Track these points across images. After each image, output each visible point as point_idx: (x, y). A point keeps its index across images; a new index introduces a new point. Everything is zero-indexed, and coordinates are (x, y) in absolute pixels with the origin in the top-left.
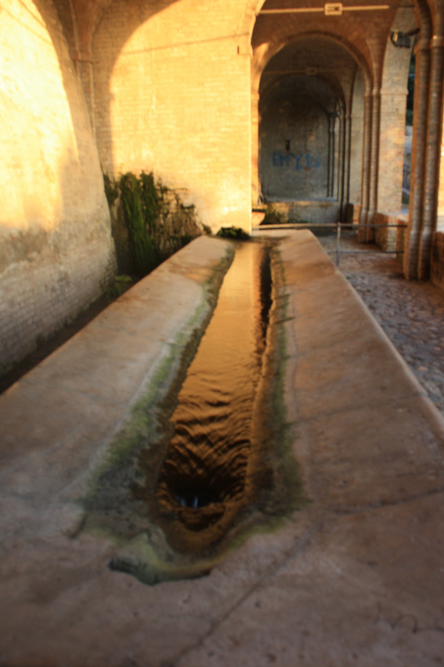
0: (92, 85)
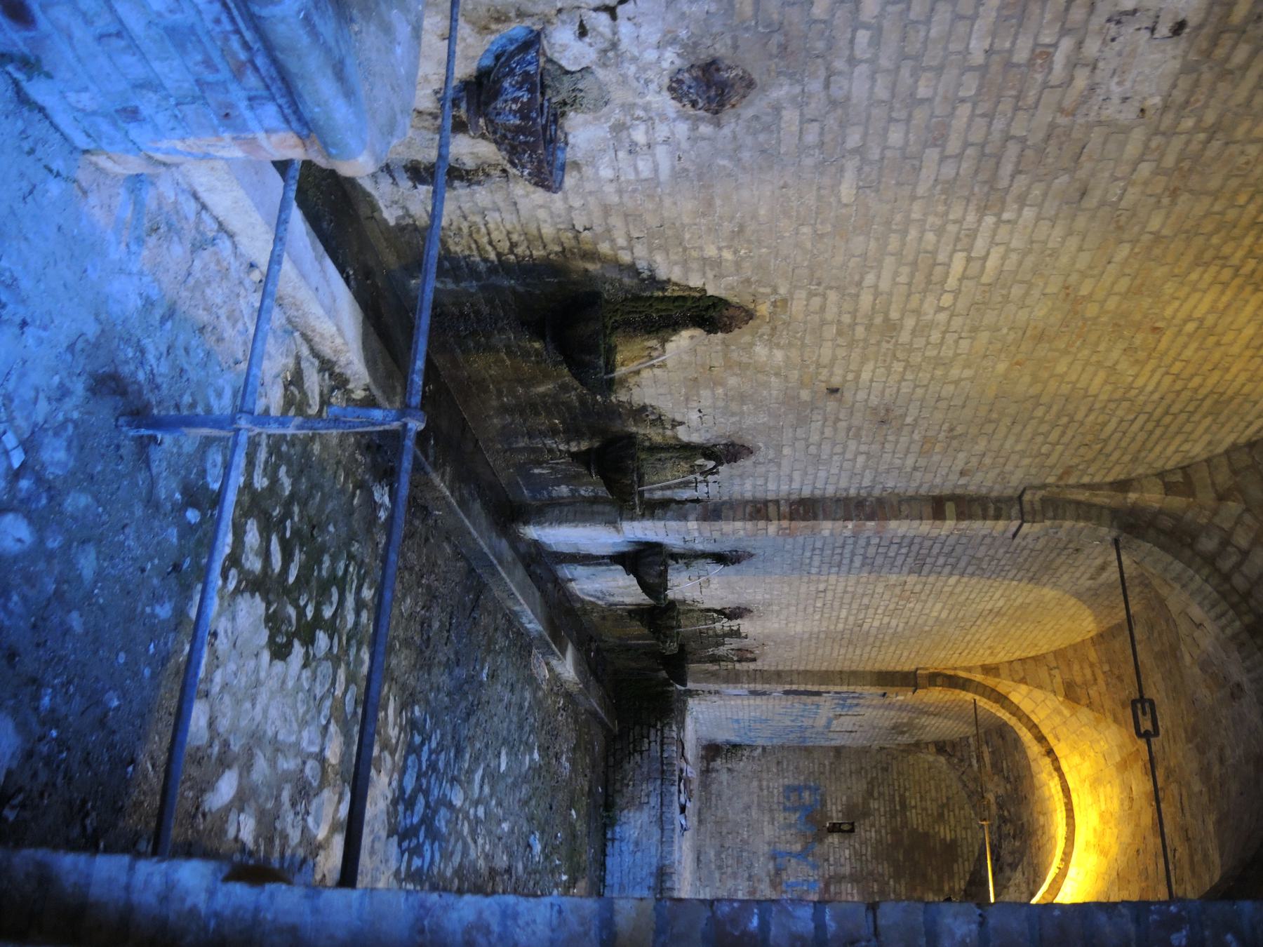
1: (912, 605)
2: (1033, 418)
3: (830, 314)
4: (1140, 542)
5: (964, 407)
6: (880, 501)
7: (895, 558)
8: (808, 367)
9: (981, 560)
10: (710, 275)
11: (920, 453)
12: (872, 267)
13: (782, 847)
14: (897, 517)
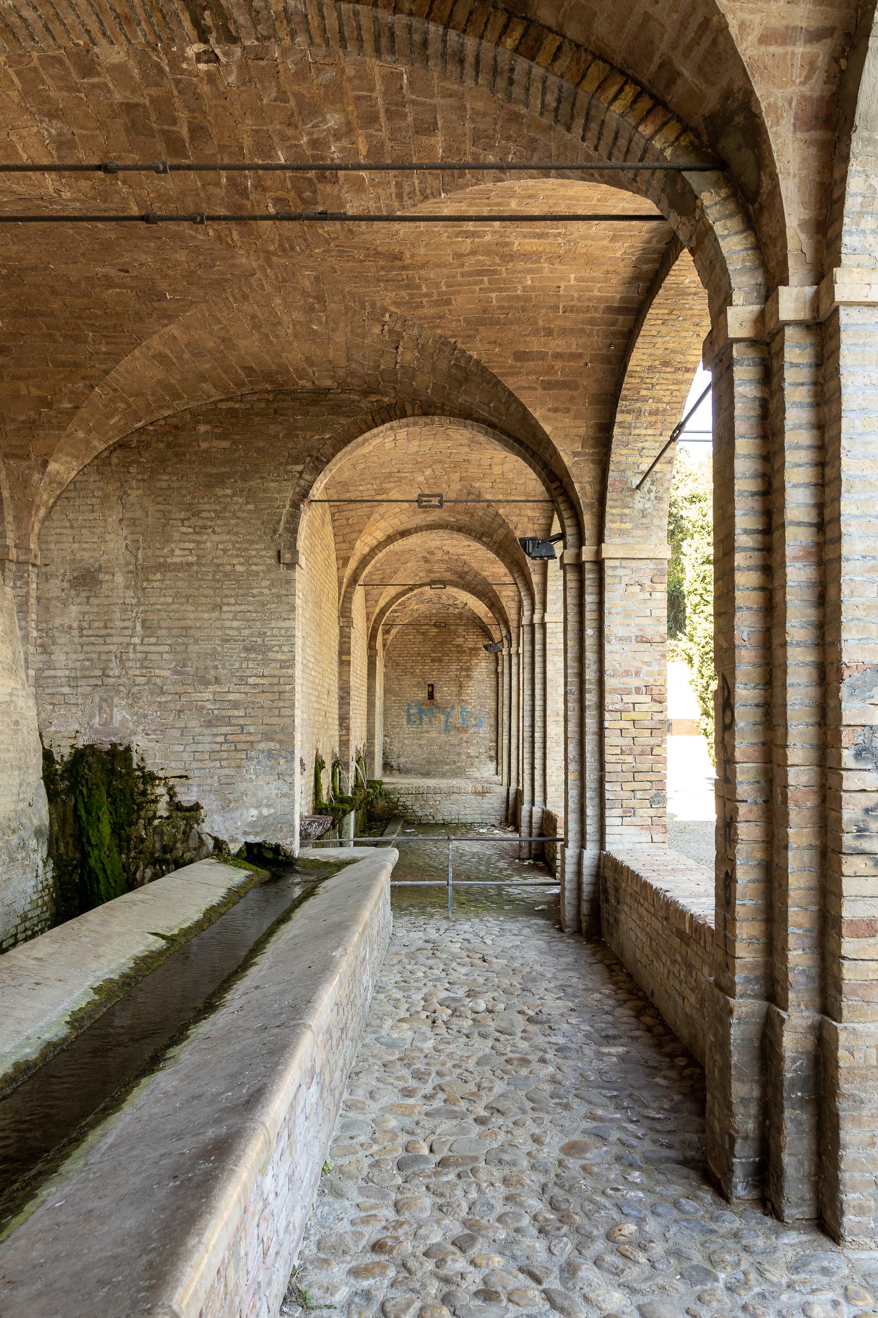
0: (33, 601)
13: (443, 727)
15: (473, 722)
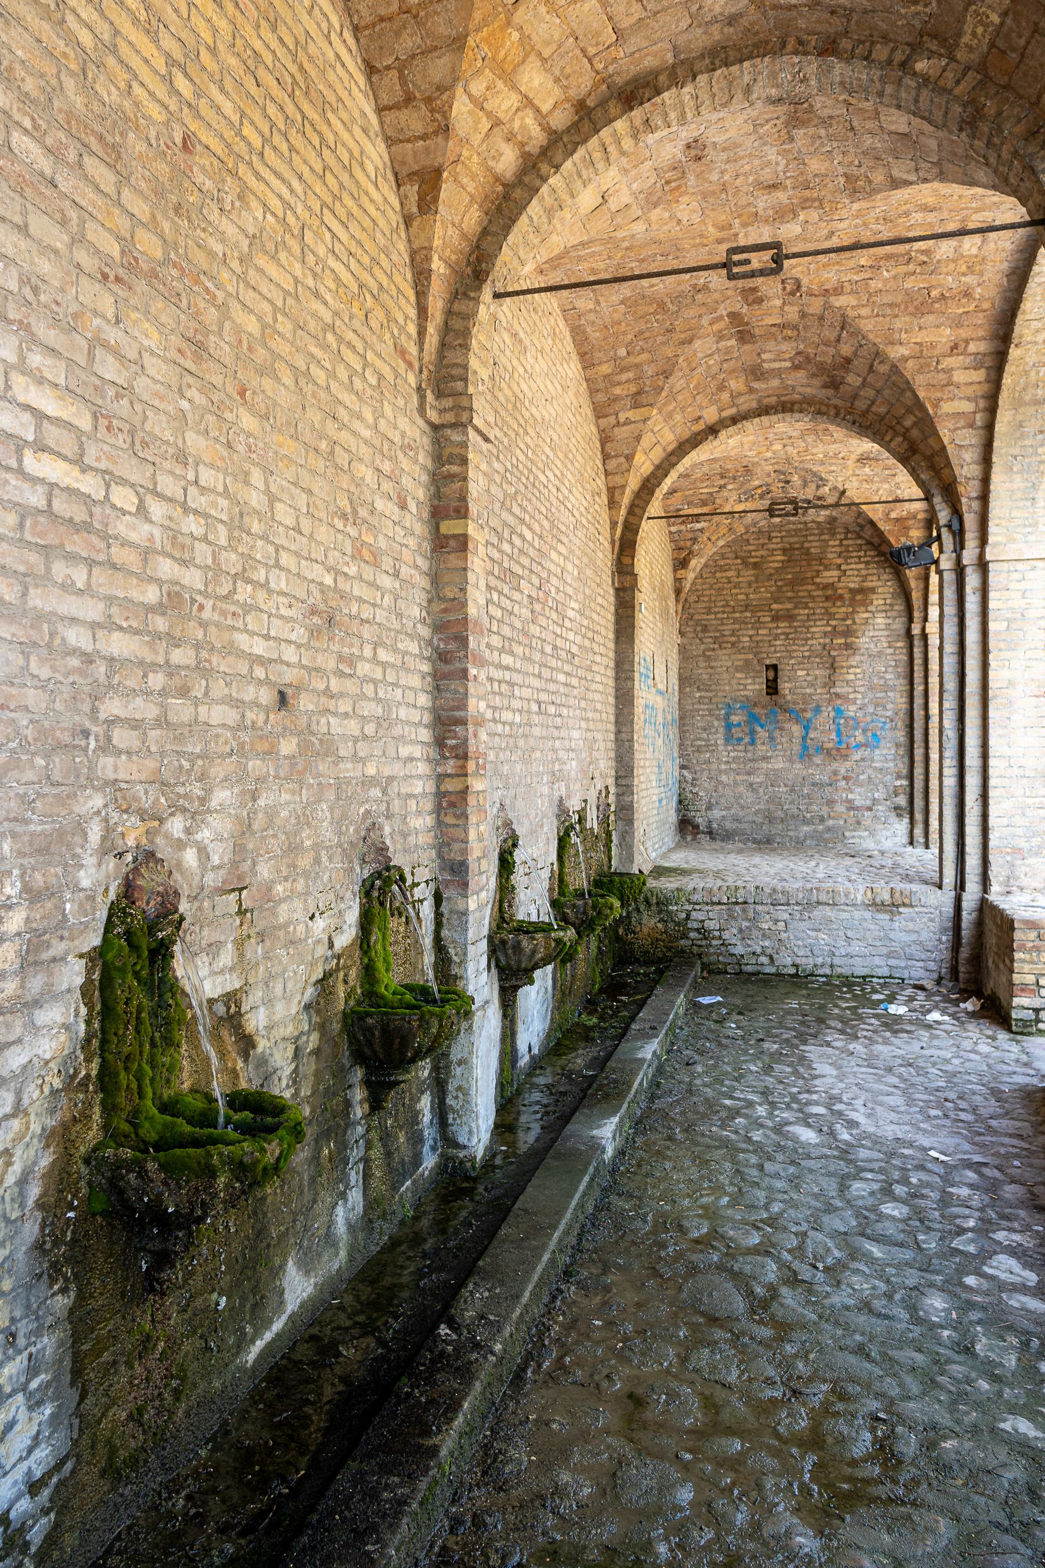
1: (553, 590)
2: (328, 388)
3: (145, 709)
4: (499, 262)
5: (309, 492)
6: (439, 627)
7: (503, 609)
8: (242, 745)
9: (506, 495)
10: (58, 948)
11: (376, 565)
12: (52, 635)
13: (796, 748)
14: (464, 605)
15: (860, 738)
